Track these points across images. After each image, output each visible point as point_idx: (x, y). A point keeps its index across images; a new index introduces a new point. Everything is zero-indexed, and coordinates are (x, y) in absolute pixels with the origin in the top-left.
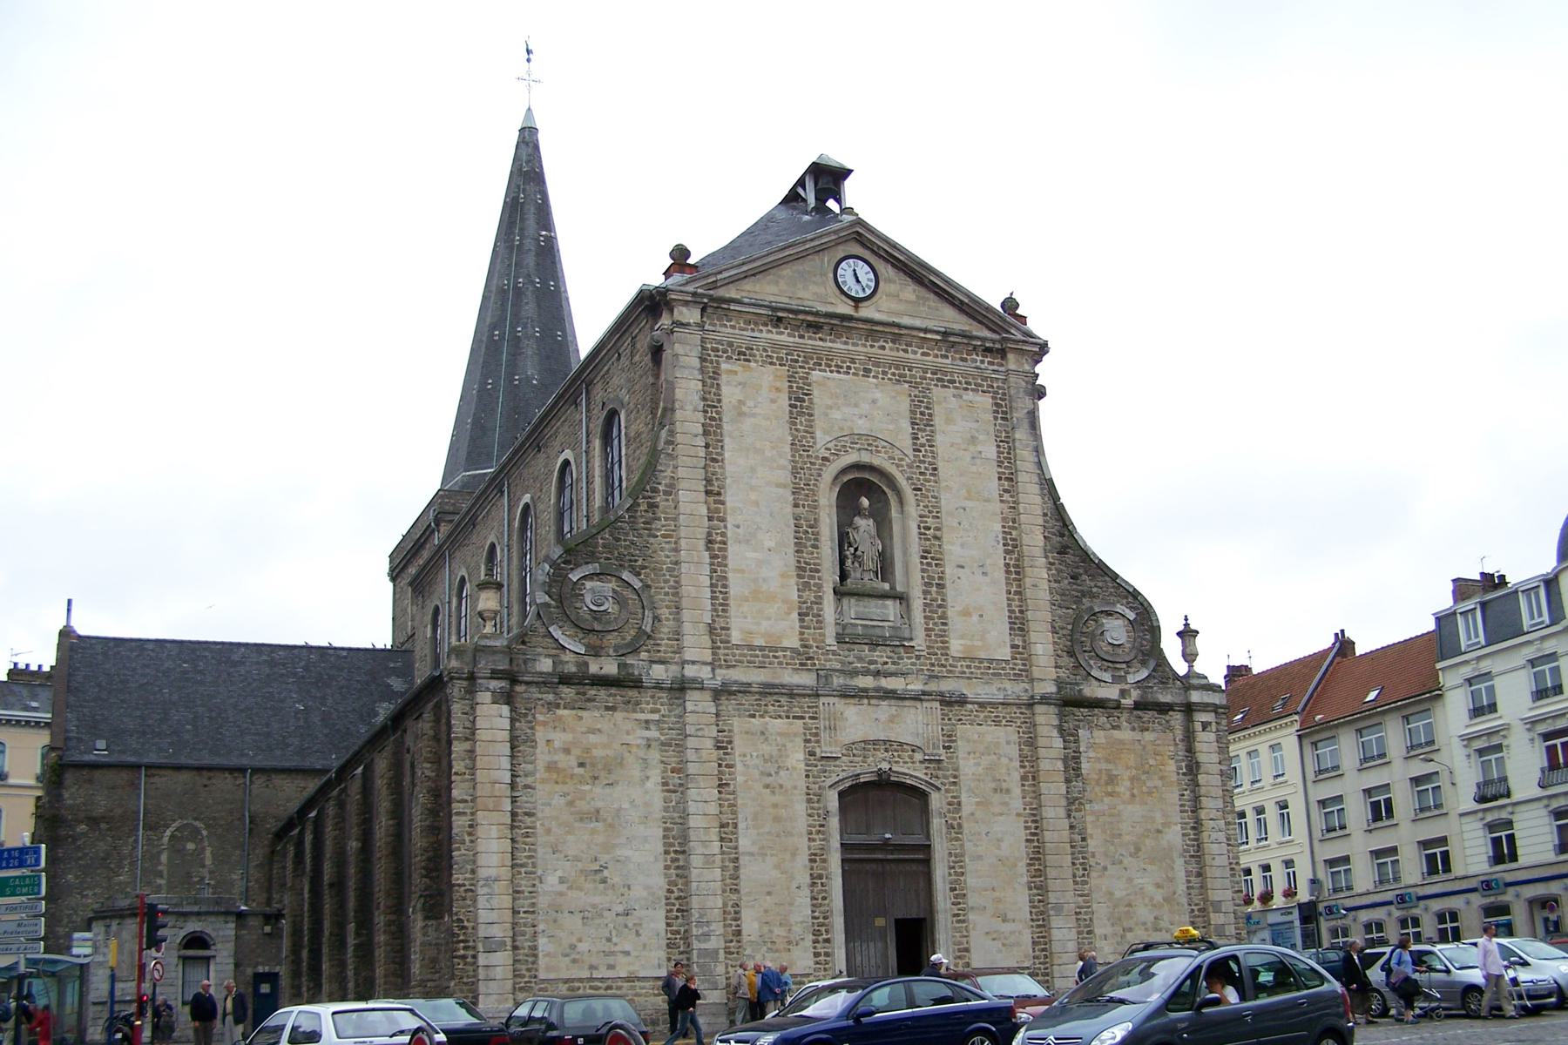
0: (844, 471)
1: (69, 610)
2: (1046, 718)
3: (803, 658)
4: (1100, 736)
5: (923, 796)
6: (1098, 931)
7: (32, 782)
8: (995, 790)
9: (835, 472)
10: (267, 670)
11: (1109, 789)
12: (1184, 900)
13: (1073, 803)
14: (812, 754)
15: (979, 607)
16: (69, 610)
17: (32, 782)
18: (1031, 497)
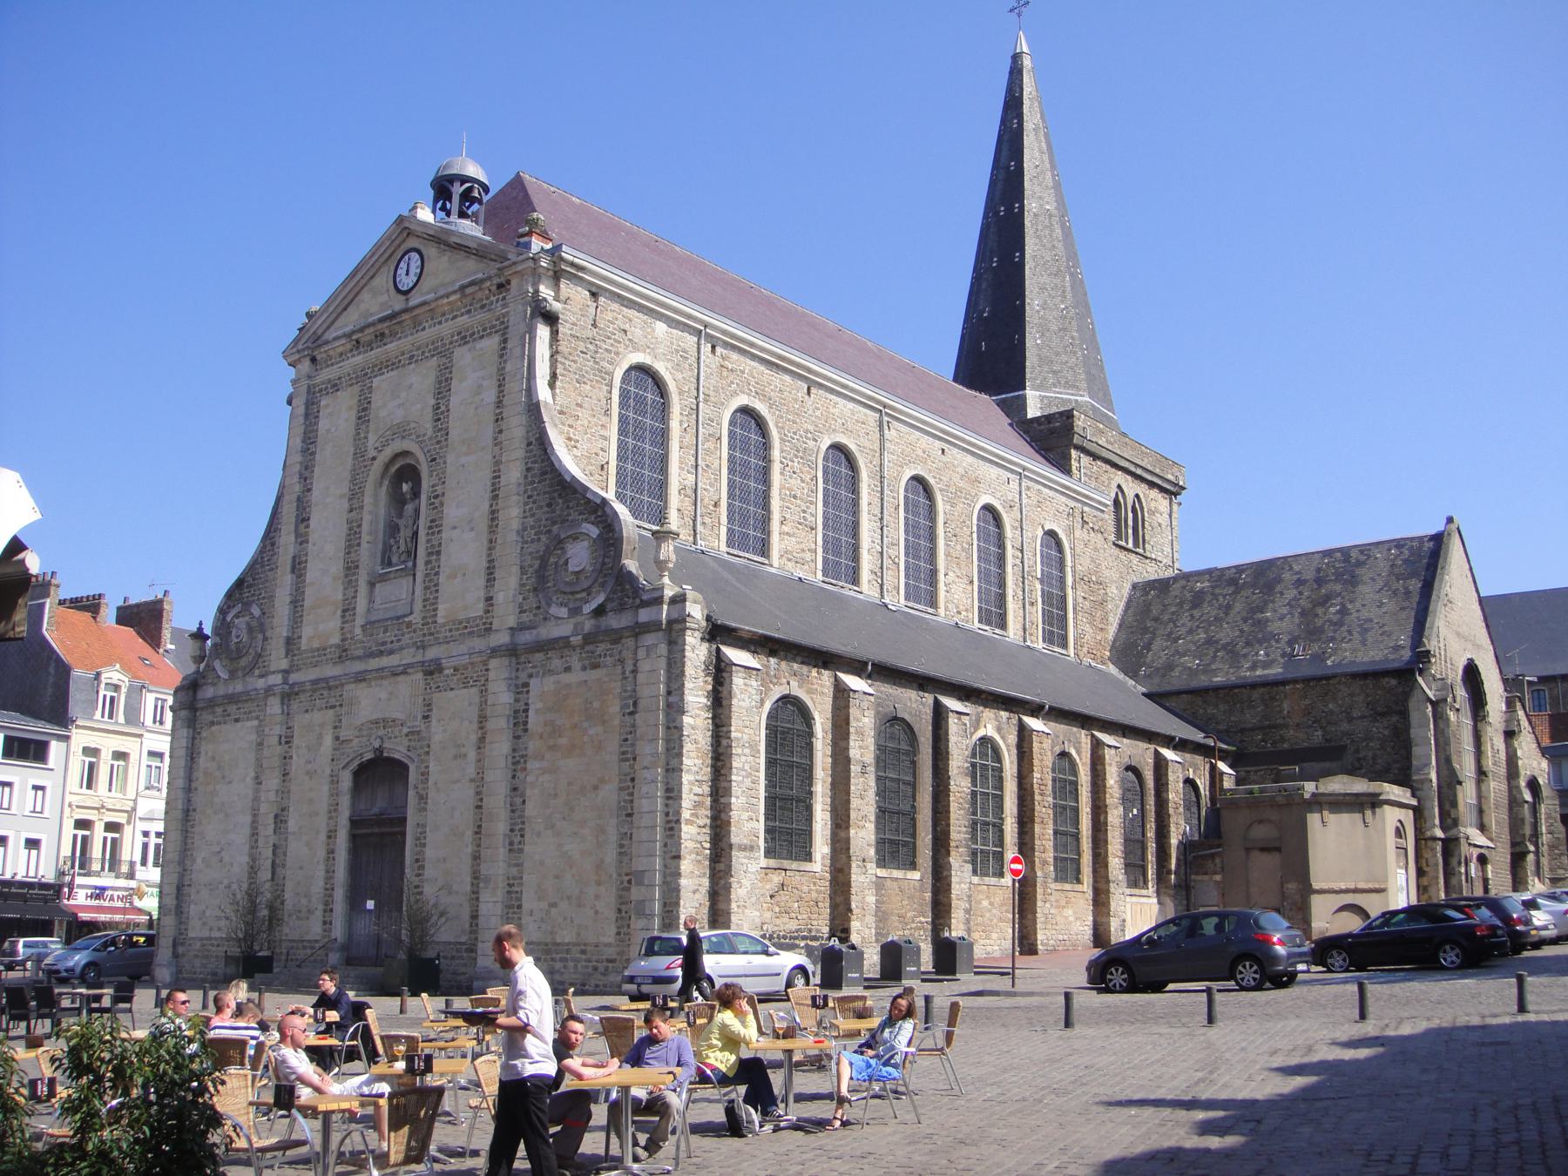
0: (387, 466)
1: (1120, 1104)
2: (499, 670)
3: (343, 654)
4: (549, 683)
5: (405, 768)
6: (526, 905)
7: (41, 873)
8: (455, 757)
9: (381, 469)
10: (669, 1029)
11: (551, 742)
12: (612, 870)
13: (518, 761)
14: (337, 738)
15: (473, 557)
16: (1120, 1104)
17: (41, 873)
18: (517, 428)
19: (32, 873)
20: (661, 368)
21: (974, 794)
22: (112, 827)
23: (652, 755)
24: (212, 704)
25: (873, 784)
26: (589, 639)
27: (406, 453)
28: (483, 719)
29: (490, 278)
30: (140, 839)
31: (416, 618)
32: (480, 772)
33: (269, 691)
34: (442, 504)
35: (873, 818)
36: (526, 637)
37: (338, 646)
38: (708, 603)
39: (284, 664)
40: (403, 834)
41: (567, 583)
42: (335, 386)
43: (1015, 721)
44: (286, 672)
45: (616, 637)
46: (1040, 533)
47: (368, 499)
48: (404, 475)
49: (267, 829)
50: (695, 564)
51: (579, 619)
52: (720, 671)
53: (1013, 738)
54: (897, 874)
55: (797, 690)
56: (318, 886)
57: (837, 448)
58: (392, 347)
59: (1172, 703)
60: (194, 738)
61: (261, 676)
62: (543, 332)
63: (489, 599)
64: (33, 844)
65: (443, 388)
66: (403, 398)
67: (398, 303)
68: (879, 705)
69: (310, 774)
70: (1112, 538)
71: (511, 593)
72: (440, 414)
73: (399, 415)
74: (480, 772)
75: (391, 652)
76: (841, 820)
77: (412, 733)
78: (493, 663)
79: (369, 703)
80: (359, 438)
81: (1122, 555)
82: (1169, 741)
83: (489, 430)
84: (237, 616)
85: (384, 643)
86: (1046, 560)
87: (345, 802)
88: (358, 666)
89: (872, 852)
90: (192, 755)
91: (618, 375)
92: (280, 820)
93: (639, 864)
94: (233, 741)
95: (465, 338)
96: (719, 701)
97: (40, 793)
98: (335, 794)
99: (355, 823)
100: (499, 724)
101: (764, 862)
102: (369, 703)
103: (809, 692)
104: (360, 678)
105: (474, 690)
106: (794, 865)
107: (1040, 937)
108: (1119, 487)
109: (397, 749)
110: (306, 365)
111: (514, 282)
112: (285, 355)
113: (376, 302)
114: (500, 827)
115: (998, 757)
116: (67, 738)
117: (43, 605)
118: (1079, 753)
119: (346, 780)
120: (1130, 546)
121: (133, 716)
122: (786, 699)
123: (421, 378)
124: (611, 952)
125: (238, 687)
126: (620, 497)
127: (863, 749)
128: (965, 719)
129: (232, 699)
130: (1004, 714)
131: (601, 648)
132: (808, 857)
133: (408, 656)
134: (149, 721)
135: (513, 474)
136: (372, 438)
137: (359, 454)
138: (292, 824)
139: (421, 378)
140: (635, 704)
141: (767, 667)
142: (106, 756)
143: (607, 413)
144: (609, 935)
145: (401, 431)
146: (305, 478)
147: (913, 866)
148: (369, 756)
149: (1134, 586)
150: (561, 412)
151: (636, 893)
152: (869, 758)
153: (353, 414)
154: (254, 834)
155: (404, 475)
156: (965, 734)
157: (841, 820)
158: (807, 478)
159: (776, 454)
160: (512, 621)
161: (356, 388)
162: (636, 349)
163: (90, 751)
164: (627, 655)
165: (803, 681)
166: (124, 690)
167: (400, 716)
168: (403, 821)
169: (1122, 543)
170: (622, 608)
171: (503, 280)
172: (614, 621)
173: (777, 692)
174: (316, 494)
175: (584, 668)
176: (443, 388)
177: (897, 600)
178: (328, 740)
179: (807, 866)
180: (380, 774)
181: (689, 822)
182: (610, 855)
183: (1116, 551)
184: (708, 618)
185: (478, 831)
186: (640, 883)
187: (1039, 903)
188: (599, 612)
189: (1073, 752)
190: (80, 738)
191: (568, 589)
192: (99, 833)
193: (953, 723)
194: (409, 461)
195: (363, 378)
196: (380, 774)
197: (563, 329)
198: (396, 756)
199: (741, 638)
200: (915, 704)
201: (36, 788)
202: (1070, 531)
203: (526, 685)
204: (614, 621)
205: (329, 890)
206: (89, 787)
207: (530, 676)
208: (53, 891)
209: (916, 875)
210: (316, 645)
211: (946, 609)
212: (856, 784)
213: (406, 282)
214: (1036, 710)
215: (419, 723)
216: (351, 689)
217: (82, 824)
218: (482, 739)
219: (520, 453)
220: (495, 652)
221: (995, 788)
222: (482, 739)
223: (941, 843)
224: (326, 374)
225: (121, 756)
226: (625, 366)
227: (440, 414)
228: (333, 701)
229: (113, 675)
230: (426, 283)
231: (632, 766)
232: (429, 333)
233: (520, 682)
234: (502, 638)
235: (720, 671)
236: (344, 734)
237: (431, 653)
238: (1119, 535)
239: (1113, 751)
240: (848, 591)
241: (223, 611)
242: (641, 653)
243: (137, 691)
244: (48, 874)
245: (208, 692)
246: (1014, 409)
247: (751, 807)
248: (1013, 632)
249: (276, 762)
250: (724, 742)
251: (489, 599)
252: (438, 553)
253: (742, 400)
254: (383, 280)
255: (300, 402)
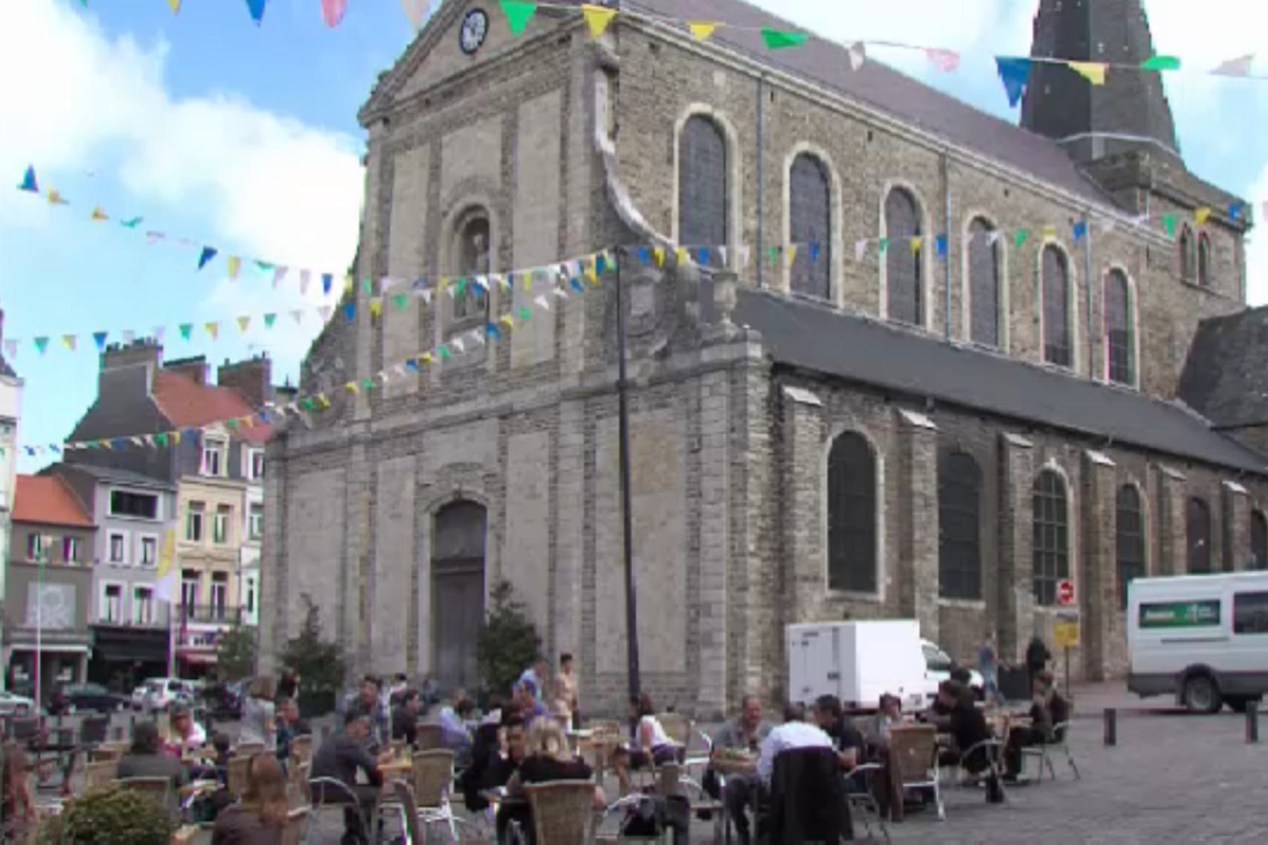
2: (570, 414)
19: (145, 620)
20: (719, 115)
21: (1037, 527)
22: (219, 576)
23: (717, 490)
24: (300, 455)
25: (936, 517)
26: (655, 382)
27: (475, 208)
28: (554, 460)
29: (550, 34)
30: (245, 588)
31: (491, 366)
32: (554, 512)
33: (353, 441)
34: (511, 255)
35: (936, 548)
36: (591, 383)
37: (416, 395)
38: (765, 343)
39: (367, 414)
40: (482, 572)
41: (634, 328)
42: (407, 145)
43: (1077, 454)
44: (368, 421)
45: (679, 378)
46: (1106, 271)
47: (442, 253)
48: (474, 226)
49: (354, 573)
50: (755, 306)
51: (645, 361)
52: (778, 407)
53: (1076, 471)
54: (962, 604)
55: (861, 428)
56: (402, 624)
57: (900, 191)
58: (461, 103)
59: (1237, 437)
60: (285, 488)
61: (346, 426)
62: (602, 84)
63: (558, 345)
64: (144, 593)
65: (508, 145)
66: (472, 151)
67: (464, 63)
68: (940, 439)
69: (397, 517)
70: (1178, 275)
71: (579, 338)
72: (507, 170)
73: (468, 172)
74: (554, 512)
75: (468, 399)
76: (905, 552)
77: (488, 476)
78: (565, 406)
79: (444, 450)
80: (433, 198)
81: (1190, 293)
82: (1234, 472)
83: (555, 183)
84: (322, 369)
85: (460, 391)
86: (1109, 299)
87: (427, 542)
88: (435, 415)
89: (936, 583)
90: (284, 504)
91: (679, 124)
92: (367, 562)
93: (706, 596)
94: (319, 487)
95: (529, 93)
96: (779, 438)
97: (149, 546)
98: (417, 537)
99: (435, 563)
100: (571, 464)
101: (830, 593)
102: (444, 450)
103: (871, 427)
104: (437, 426)
105: (545, 433)
106: (858, 596)
107: (1106, 664)
108: (1185, 225)
109: (476, 490)
110: (379, 126)
111: (575, 37)
112: (360, 117)
113: (445, 62)
114: (575, 561)
115: (1060, 489)
116: (174, 493)
117: (144, 369)
118: (1143, 484)
119: (427, 522)
120: (1197, 282)
121: (235, 472)
122: (847, 434)
123: (487, 135)
124: (681, 682)
125: (323, 438)
126: (682, 242)
127: (926, 483)
128: (1029, 453)
129: (325, 449)
130: (1067, 447)
131: (666, 388)
132: (871, 586)
133: (481, 403)
134: (250, 476)
135: (579, 222)
136: (444, 194)
137: (432, 209)
138: (379, 566)
139: (487, 135)
140: (700, 442)
141: (828, 403)
142: (211, 507)
143: (670, 161)
144: (679, 664)
145: (471, 184)
146: (383, 233)
147: (975, 595)
148: (450, 499)
149: (1202, 323)
150: (623, 162)
151: (704, 624)
152: (932, 490)
153: (425, 173)
154: (343, 578)
155: (474, 226)
156: (1026, 466)
157: (905, 552)
158: (869, 221)
159: (838, 198)
160: (581, 365)
161: (427, 146)
162: (695, 97)
163: (197, 505)
164: (693, 394)
165: (865, 416)
166: (226, 446)
167: (476, 459)
168: (481, 560)
169: (1189, 280)
170: (687, 348)
171: (563, 34)
172: (681, 362)
173: (837, 430)
174: (392, 251)
175: (650, 409)
176: (508, 145)
177: (964, 340)
178: (410, 485)
179: (869, 597)
180: (459, 514)
181: (753, 554)
182: (681, 587)
183: (1181, 289)
184: (769, 357)
185: (552, 569)
186: (709, 614)
187: (1105, 632)
188: (663, 355)
189: (1138, 484)
190: (187, 493)
191: (634, 333)
192: (206, 583)
193: (1014, 456)
194: (480, 215)
195: (433, 137)
196: (459, 514)
197: (624, 81)
198: (475, 499)
199: (799, 376)
200: (975, 437)
201: (146, 540)
202: (1135, 270)
203: (594, 427)
204: (681, 362)
205: (413, 625)
206: (197, 537)
207: (599, 417)
208: (160, 637)
209: (981, 605)
210: (397, 393)
211: (1012, 347)
212: (920, 516)
213: (470, 40)
214: (1099, 442)
215: (496, 468)
216: (434, 437)
217: (188, 574)
218: (555, 480)
219: (586, 202)
220: (566, 396)
221: (1059, 520)
222: (555, 480)
223: (1005, 573)
224: (399, 133)
225: (224, 508)
226: (686, 115)
227: (507, 170)
228: (413, 447)
229: (216, 431)
230: (493, 41)
231: (697, 502)
232: (494, 87)
233: (588, 424)
234: (571, 382)
235: (778, 407)
236: (425, 479)
237: (505, 399)
238: (1185, 271)
239: (1178, 484)
240: (917, 332)
241: (306, 365)
242: (705, 392)
243: (235, 447)
244: (155, 619)
245: (296, 443)
246: (1078, 154)
247: (813, 540)
248: (1079, 367)
249: (363, 506)
250: (787, 476)
251: (558, 345)
252: (510, 302)
253: (803, 146)
254: (449, 41)
255: (375, 161)
